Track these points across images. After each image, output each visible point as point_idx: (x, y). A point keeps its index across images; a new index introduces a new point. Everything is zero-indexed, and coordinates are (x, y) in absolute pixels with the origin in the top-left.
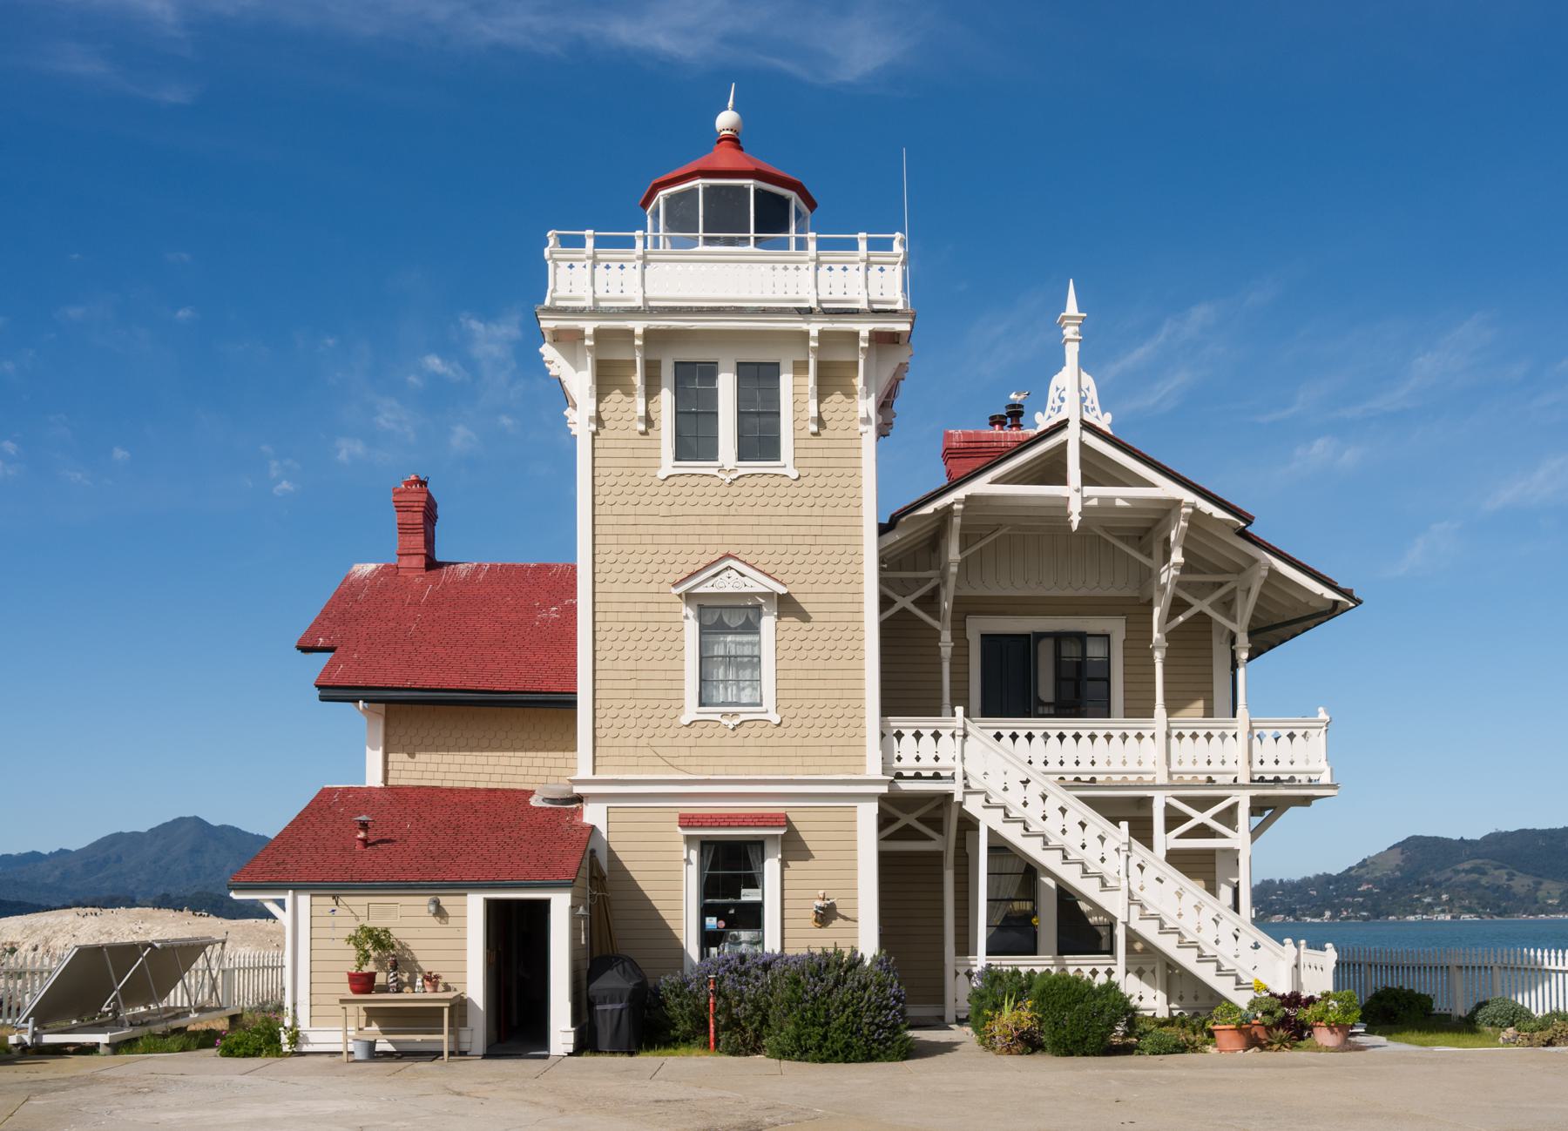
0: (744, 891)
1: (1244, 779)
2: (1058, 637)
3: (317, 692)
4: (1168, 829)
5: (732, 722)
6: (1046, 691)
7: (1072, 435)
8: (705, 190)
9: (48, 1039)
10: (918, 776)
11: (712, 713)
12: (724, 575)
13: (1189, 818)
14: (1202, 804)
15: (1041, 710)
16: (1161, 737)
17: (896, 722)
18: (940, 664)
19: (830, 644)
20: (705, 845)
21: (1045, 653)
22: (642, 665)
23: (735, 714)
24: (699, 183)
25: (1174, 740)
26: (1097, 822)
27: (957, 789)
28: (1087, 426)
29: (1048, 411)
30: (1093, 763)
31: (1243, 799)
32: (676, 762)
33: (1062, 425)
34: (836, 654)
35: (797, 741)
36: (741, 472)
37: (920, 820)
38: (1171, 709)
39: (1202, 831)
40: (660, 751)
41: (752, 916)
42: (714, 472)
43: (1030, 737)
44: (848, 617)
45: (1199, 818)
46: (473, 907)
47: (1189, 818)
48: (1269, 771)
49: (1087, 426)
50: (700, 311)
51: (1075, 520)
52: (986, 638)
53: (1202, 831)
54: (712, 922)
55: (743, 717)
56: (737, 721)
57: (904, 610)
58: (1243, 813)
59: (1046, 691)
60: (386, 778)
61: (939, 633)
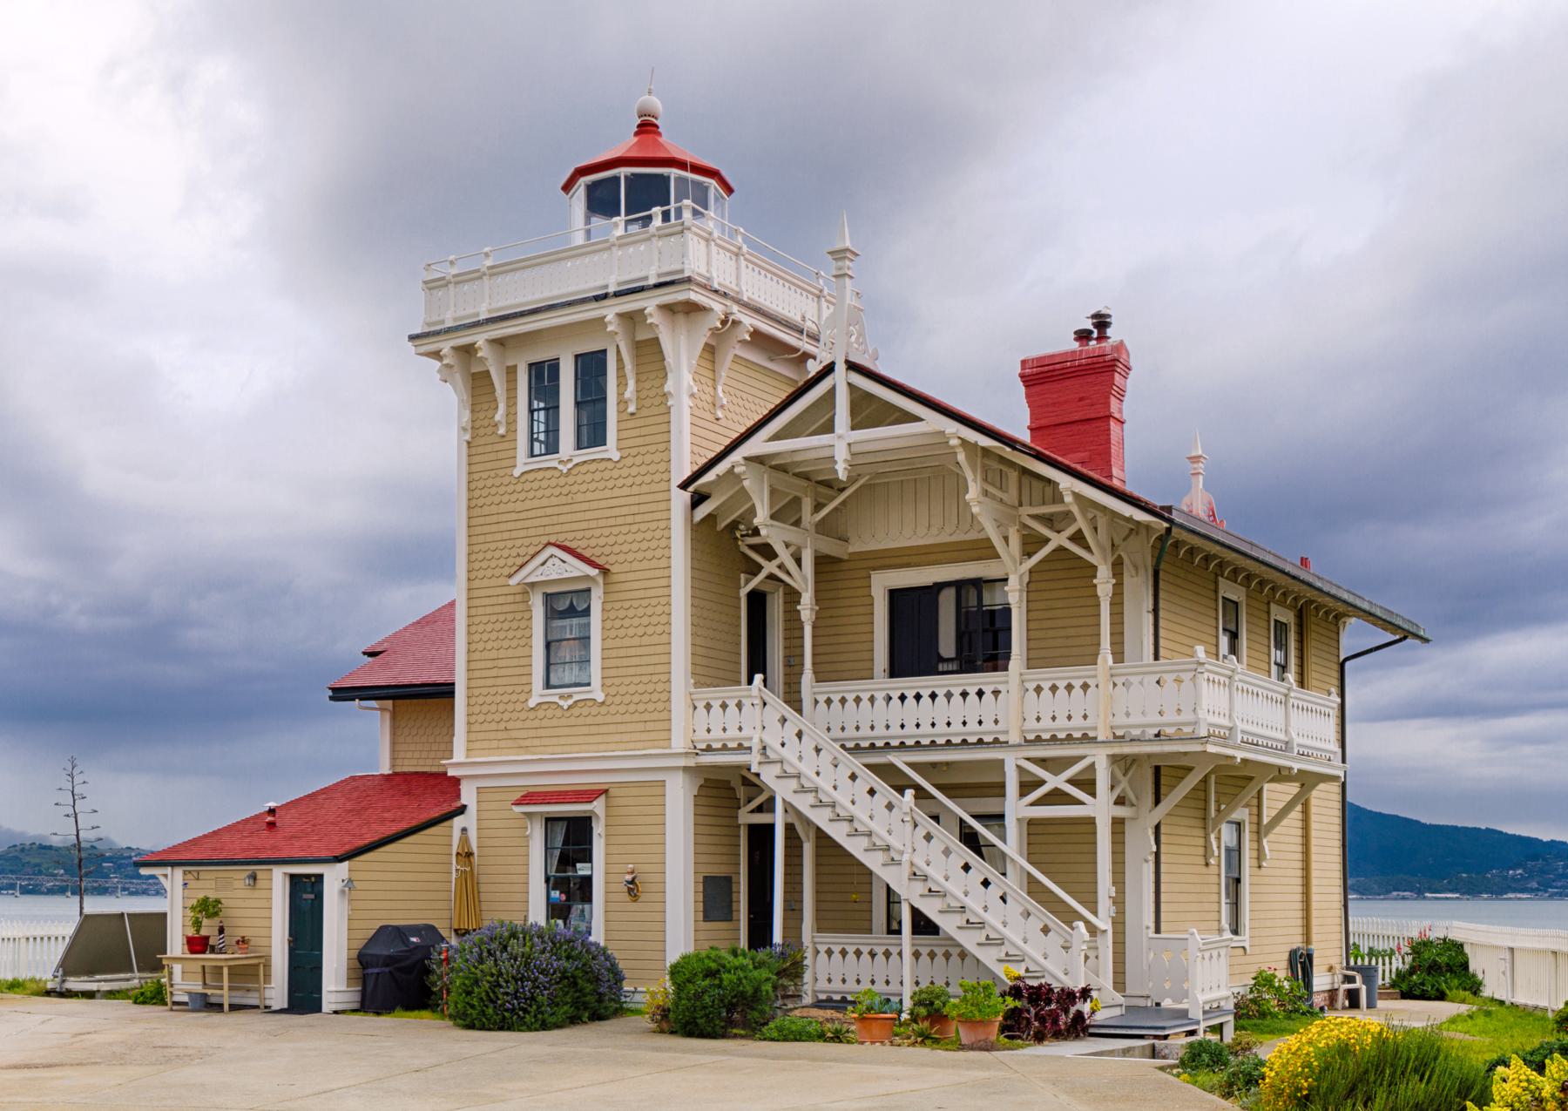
1: (1014, 738)
2: (959, 585)
4: (1022, 795)
5: (565, 704)
6: (947, 647)
7: (840, 377)
9: (74, 984)
11: (553, 696)
12: (549, 563)
18: (802, 629)
21: (947, 601)
23: (570, 696)
24: (623, 172)
26: (885, 791)
27: (753, 760)
28: (852, 366)
30: (724, 730)
31: (1099, 758)
33: (829, 369)
37: (1070, 781)
38: (1031, 663)
39: (1057, 797)
42: (555, 464)
44: (660, 592)
45: (1054, 782)
46: (278, 880)
47: (1042, 782)
48: (1046, 727)
49: (852, 366)
50: (522, 314)
52: (893, 594)
53: (1057, 797)
54: (556, 894)
55: (576, 698)
56: (570, 702)
57: (1061, 549)
59: (947, 647)
60: (393, 766)
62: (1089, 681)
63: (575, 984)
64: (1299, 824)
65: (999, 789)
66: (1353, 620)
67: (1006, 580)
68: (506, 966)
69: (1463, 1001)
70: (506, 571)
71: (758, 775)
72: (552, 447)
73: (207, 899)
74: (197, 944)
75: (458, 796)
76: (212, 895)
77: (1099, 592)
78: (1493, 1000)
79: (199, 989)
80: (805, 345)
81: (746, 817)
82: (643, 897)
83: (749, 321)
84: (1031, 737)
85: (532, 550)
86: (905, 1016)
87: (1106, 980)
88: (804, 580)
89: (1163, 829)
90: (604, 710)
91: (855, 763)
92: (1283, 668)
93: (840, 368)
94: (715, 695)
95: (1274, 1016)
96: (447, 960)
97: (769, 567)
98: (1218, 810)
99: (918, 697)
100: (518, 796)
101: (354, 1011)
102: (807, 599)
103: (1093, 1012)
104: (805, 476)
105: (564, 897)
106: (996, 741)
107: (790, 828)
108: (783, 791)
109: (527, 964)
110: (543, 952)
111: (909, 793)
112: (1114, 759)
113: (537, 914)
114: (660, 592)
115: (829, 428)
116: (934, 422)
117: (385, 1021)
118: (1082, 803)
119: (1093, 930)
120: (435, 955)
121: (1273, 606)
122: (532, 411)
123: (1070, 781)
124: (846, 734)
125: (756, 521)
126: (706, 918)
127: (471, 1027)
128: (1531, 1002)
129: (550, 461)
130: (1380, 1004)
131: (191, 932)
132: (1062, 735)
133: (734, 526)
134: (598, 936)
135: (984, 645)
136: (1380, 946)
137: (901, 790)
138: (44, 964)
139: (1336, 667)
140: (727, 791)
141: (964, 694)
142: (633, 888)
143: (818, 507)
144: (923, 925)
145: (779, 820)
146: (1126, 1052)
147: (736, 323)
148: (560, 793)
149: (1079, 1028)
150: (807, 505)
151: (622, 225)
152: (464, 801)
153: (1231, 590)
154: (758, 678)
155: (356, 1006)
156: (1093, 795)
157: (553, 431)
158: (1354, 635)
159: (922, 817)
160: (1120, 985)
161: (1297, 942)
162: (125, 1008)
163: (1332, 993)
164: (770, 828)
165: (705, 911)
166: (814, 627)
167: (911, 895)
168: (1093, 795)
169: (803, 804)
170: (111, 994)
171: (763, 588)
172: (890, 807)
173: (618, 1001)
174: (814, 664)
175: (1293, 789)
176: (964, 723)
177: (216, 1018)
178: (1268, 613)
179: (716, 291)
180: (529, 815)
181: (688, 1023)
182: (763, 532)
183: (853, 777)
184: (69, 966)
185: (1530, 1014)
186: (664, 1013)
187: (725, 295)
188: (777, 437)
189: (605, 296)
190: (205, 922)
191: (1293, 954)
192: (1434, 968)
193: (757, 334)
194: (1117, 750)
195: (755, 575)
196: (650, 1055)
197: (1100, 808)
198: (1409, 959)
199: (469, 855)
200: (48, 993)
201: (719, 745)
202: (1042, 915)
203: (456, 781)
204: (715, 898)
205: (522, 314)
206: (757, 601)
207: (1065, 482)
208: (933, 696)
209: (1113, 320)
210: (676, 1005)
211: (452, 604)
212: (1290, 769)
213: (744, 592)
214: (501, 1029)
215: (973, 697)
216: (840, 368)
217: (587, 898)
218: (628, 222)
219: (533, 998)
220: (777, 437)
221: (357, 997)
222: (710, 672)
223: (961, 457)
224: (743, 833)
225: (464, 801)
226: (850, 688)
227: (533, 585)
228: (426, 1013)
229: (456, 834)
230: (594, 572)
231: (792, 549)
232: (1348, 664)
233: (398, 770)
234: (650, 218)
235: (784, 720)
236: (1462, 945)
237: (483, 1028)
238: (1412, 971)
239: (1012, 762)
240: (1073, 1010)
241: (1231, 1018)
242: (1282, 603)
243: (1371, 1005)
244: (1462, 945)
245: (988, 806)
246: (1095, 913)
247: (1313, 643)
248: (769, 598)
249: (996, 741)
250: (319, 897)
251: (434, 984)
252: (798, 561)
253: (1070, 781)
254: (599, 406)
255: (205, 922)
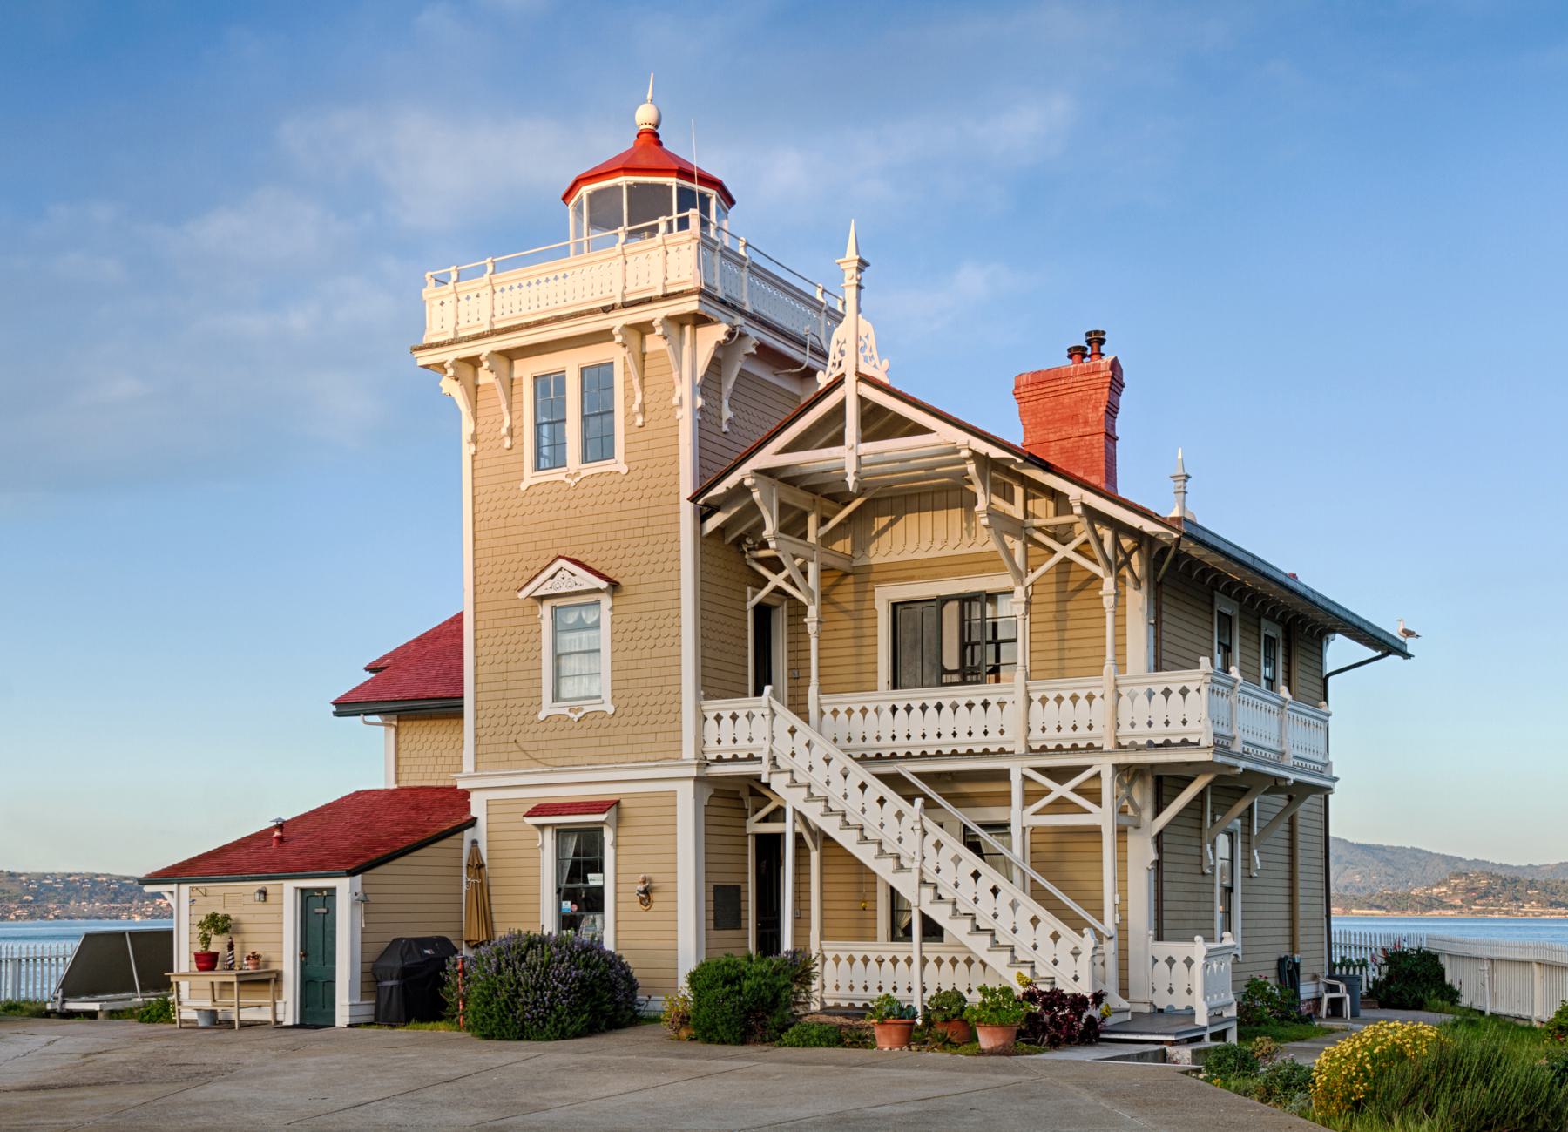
0: (590, 876)
2: (966, 600)
3: (334, 708)
6: (951, 660)
7: (850, 392)
8: (629, 187)
9: (72, 1006)
10: (735, 759)
13: (1049, 791)
14: (1060, 775)
15: (945, 679)
16: (1110, 697)
17: (712, 707)
19: (655, 633)
20: (561, 832)
22: (512, 666)
23: (580, 709)
24: (623, 181)
25: (1036, 705)
26: (895, 800)
27: (763, 770)
28: (863, 378)
29: (829, 368)
31: (1104, 765)
32: (538, 755)
33: (839, 382)
34: (660, 642)
35: (629, 729)
36: (584, 473)
39: (1061, 805)
40: (525, 746)
41: (593, 901)
42: (561, 477)
43: (734, 717)
47: (1049, 791)
48: (1051, 739)
50: (528, 326)
51: (851, 480)
53: (1061, 805)
54: (567, 905)
55: (587, 709)
56: (580, 714)
58: (1107, 786)
60: (397, 781)
61: (805, 608)
62: (1094, 692)
63: (594, 992)
64: (1286, 835)
65: (1006, 798)
66: (1338, 636)
67: (1012, 592)
68: (523, 976)
69: (1441, 1011)
70: (515, 585)
71: (767, 786)
72: (558, 461)
73: (214, 916)
74: (207, 961)
75: (468, 808)
76: (221, 912)
77: (1105, 604)
78: (1471, 1010)
79: (207, 1004)
80: (807, 359)
81: (755, 827)
82: (655, 906)
83: (755, 334)
84: (1036, 746)
85: (541, 564)
86: (919, 1022)
87: (1111, 989)
88: (808, 591)
89: (1165, 838)
90: (615, 721)
91: (860, 773)
92: (1271, 682)
93: (851, 379)
94: (725, 706)
95: (1266, 1022)
96: (463, 971)
97: (776, 580)
98: (1213, 821)
99: (924, 708)
100: (529, 808)
101: (368, 1024)
102: (813, 611)
103: (1104, 1018)
104: (812, 489)
105: (575, 908)
106: (1002, 751)
107: (799, 838)
108: (792, 800)
109: (546, 974)
110: (561, 961)
111: (919, 802)
112: (1118, 768)
113: (548, 924)
114: (669, 604)
115: (839, 440)
116: (945, 434)
117: (402, 1033)
118: (1087, 812)
119: (1099, 936)
120: (449, 967)
121: (1264, 622)
122: (538, 426)
123: (1074, 790)
124: (852, 745)
125: (765, 534)
126: (717, 926)
127: (486, 1037)
128: (1513, 1012)
129: (557, 475)
130: (1363, 1013)
131: (199, 948)
132: (1067, 745)
133: (739, 541)
134: (609, 945)
135: (979, 660)
136: (1354, 956)
137: (910, 800)
138: (44, 987)
139: (1319, 682)
140: (734, 798)
141: (970, 706)
142: (647, 894)
143: (823, 521)
144: (932, 930)
145: (788, 828)
146: (1141, 1057)
147: (742, 336)
148: (577, 804)
149: (1091, 1035)
150: (812, 520)
151: (622, 237)
152: (473, 813)
153: (1225, 606)
154: (768, 689)
155: (371, 1019)
156: (1099, 804)
157: (558, 445)
158: (1339, 650)
159: (929, 825)
160: (1124, 991)
161: (1284, 951)
162: (134, 1028)
163: (1317, 1001)
164: (777, 839)
165: (715, 919)
166: (819, 640)
167: (920, 902)
168: (1099, 804)
169: (814, 813)
170: (113, 1014)
171: (770, 602)
172: (900, 815)
173: (632, 1009)
174: (819, 676)
175: (1281, 800)
176: (986, 733)
177: (228, 1035)
178: (1259, 628)
179: (723, 302)
180: (542, 827)
181: (708, 1029)
182: (772, 545)
183: (863, 786)
184: (71, 987)
185: (1508, 1026)
186: (684, 1020)
187: (733, 307)
188: (786, 450)
189: (613, 307)
190: (214, 938)
191: (1281, 961)
192: (1411, 976)
193: (762, 348)
194: (1123, 759)
195: (762, 588)
196: (675, 1062)
197: (1103, 816)
198: (1385, 969)
199: (481, 866)
200: (48, 1014)
201: (729, 756)
202: (1050, 922)
203: (466, 794)
204: (722, 906)
205: (528, 326)
206: (763, 614)
207: (1074, 492)
208: (939, 707)
209: (1107, 337)
210: (697, 1010)
211: (459, 619)
212: (1287, 779)
213: (750, 604)
214: (520, 1039)
215: (978, 708)
216: (851, 379)
217: (599, 908)
218: (631, 234)
219: (552, 1008)
220: (786, 450)
221: (370, 1010)
222: (715, 683)
223: (971, 468)
224: (751, 842)
225: (473, 813)
226: (856, 700)
227: (542, 598)
228: (441, 1029)
229: (467, 846)
230: (603, 585)
231: (799, 561)
232: (1331, 679)
233: (403, 784)
234: (655, 229)
235: (793, 731)
236: (1436, 957)
237: (502, 1038)
238: (1389, 978)
239: (1017, 769)
240: (1085, 1015)
241: (1234, 1024)
242: (1271, 618)
243: (1354, 1014)
244: (1436, 957)
245: (995, 814)
246: (1101, 920)
247: (1300, 658)
248: (774, 614)
249: (1002, 751)
250: (331, 912)
251: (450, 995)
252: (805, 573)
253: (1074, 790)
254: (606, 418)
255: (214, 938)
